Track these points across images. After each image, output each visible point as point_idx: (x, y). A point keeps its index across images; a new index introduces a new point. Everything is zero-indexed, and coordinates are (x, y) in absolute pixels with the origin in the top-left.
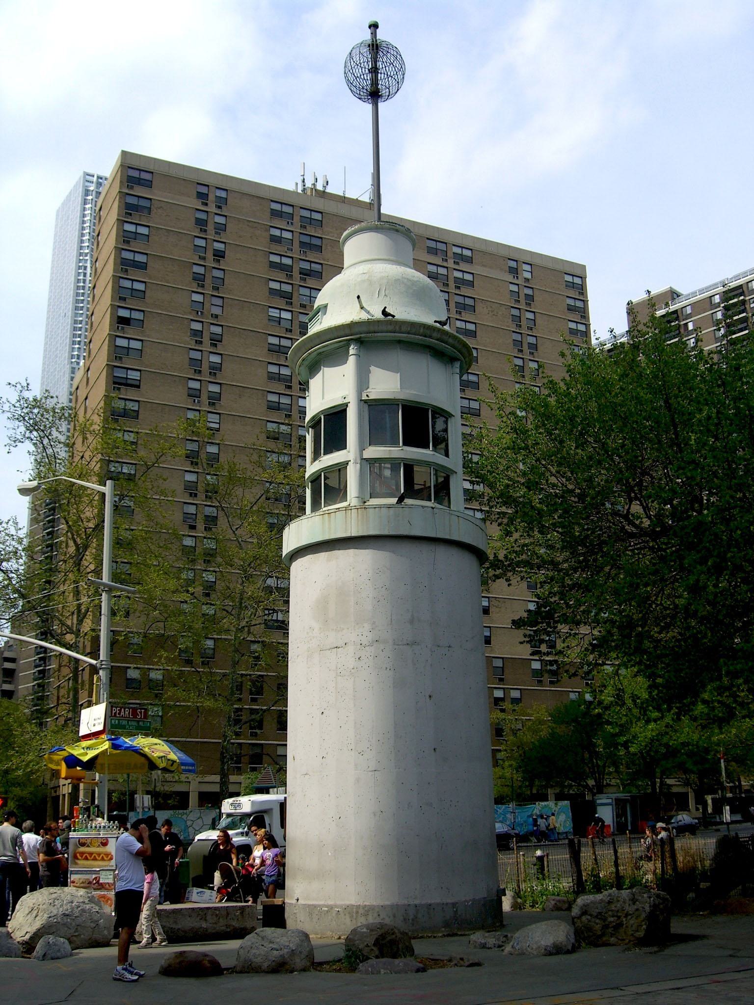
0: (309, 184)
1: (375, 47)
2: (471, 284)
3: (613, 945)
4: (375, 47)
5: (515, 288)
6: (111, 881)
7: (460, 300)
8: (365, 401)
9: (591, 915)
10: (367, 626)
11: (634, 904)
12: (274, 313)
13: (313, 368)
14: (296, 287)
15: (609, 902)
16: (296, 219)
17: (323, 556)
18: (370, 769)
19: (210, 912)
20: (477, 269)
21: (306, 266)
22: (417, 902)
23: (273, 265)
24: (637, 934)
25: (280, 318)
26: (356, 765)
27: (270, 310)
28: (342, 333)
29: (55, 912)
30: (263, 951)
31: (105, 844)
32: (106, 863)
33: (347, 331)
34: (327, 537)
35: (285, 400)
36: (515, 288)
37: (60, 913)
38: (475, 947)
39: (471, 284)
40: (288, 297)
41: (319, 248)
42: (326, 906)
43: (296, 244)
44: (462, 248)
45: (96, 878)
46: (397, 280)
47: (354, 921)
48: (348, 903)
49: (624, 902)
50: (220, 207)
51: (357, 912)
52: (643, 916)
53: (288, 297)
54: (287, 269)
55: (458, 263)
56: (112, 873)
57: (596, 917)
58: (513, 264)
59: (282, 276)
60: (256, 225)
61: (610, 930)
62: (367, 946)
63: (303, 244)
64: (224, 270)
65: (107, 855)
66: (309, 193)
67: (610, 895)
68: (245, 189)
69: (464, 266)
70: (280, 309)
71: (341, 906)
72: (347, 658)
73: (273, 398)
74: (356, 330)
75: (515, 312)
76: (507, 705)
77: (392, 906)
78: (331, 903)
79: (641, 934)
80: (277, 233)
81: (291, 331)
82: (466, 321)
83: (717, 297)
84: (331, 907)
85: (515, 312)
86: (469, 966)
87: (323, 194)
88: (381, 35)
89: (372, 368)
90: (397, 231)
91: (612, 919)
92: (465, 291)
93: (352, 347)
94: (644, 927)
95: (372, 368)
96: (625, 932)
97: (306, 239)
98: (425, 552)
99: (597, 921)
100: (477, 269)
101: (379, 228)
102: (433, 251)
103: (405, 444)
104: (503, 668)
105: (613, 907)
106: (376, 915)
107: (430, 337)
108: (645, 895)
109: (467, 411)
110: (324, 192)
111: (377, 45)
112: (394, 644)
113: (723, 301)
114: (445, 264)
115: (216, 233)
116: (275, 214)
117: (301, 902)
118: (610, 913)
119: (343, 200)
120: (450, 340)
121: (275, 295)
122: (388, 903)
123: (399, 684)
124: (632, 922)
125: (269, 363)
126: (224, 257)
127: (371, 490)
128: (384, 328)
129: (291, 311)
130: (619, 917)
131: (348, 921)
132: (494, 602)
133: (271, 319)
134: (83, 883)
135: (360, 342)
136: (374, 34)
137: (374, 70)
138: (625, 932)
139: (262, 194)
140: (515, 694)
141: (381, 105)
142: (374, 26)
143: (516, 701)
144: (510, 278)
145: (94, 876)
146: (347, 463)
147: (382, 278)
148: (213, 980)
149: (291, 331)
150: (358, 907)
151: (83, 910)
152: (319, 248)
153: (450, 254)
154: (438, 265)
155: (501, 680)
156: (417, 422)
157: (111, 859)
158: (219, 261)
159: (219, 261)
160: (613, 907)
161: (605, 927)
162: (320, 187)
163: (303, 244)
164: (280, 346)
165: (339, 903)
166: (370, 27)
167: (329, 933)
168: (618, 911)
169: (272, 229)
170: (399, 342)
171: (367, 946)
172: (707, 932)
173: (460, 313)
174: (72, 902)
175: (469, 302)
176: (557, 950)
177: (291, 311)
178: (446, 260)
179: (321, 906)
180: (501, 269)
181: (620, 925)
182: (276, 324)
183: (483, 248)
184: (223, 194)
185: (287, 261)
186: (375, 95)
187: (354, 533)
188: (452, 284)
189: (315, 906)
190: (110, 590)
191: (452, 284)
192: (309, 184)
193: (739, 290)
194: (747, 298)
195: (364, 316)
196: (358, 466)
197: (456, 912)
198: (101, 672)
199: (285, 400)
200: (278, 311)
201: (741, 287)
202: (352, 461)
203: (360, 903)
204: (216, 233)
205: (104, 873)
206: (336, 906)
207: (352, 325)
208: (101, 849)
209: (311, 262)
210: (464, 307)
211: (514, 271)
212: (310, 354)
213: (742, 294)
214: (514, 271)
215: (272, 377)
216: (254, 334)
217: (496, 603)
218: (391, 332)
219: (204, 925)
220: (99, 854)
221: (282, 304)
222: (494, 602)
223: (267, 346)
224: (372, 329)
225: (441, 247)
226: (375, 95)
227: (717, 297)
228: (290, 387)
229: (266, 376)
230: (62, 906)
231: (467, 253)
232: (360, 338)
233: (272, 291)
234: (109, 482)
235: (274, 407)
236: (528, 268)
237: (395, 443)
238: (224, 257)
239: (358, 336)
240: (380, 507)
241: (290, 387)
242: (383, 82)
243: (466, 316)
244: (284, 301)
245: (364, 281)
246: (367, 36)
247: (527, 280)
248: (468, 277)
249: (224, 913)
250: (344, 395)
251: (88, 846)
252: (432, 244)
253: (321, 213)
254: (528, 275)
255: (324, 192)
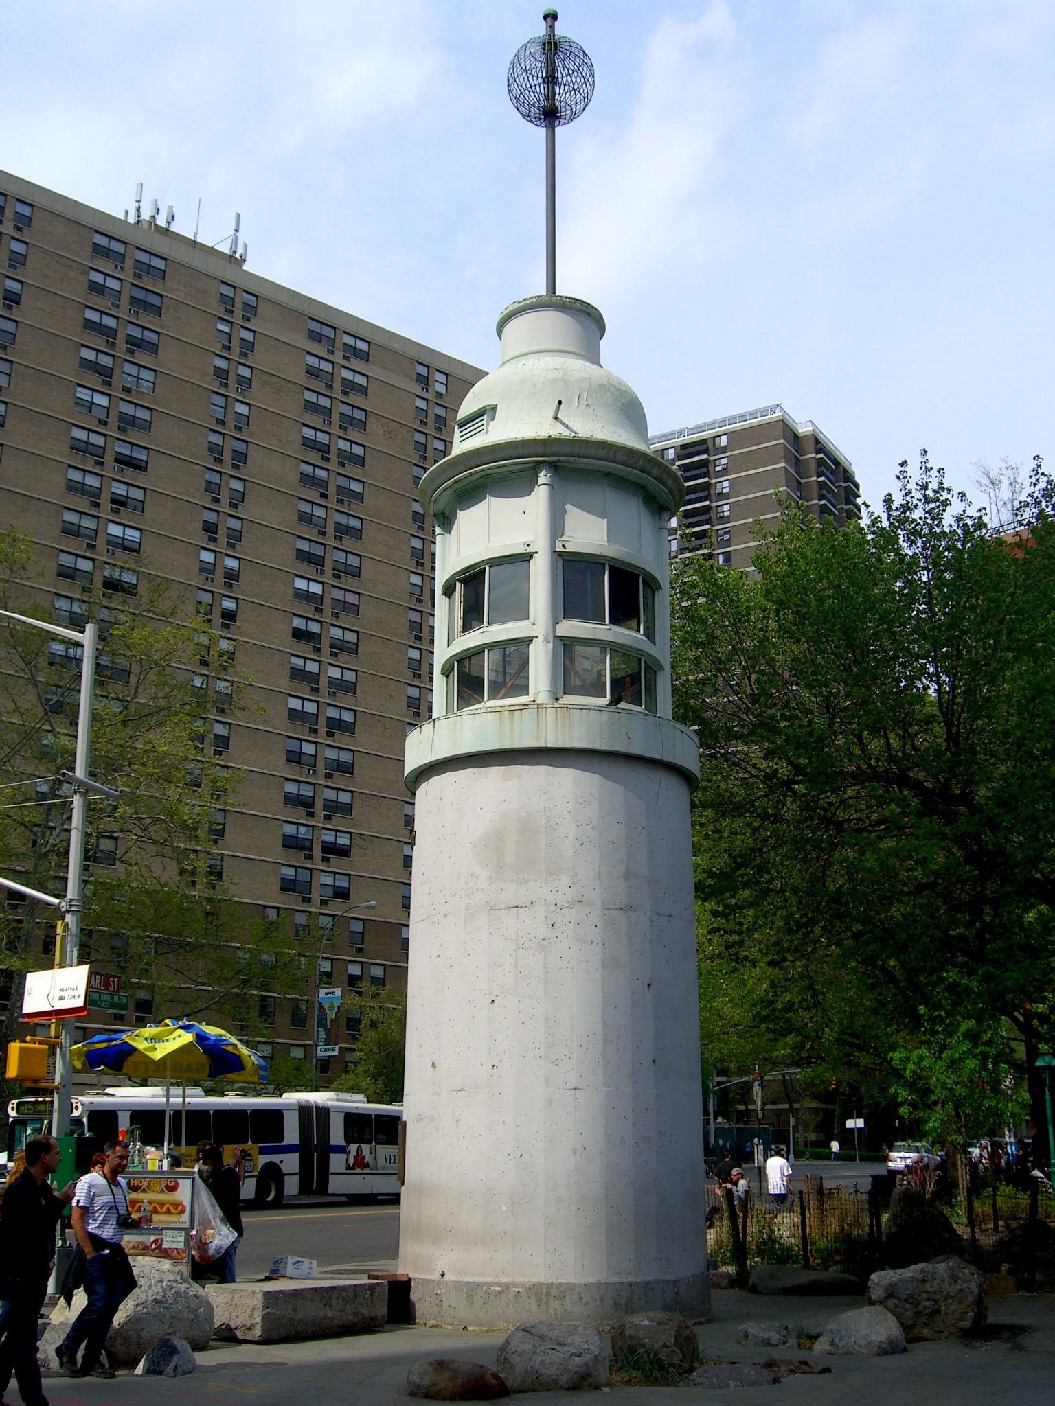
0: (146, 215)
1: (552, 47)
2: (364, 391)
3: (927, 1340)
4: (552, 47)
5: (421, 404)
6: (181, 1246)
7: (347, 410)
8: (560, 554)
9: (899, 1299)
10: (565, 879)
11: (955, 1282)
12: (84, 394)
13: (469, 494)
14: (118, 361)
15: (923, 1281)
16: (129, 263)
17: (494, 773)
18: (568, 1086)
19: (335, 1294)
20: (372, 370)
21: (136, 333)
22: (631, 1279)
23: (89, 324)
24: (961, 1324)
25: (92, 402)
26: (547, 1080)
27: (79, 389)
28: (532, 451)
29: (144, 1298)
30: (555, 1357)
31: (172, 1189)
32: (175, 1218)
33: (540, 450)
34: (507, 744)
35: (88, 523)
36: (421, 404)
37: (151, 1299)
38: (756, 1344)
39: (364, 391)
40: (106, 374)
41: (158, 311)
42: (499, 1285)
43: (125, 299)
44: (356, 337)
45: (155, 1241)
46: (602, 386)
47: (543, 1307)
48: (534, 1280)
49: (942, 1281)
50: (20, 229)
51: (548, 1294)
52: (970, 1299)
53: (106, 374)
54: (109, 333)
55: (348, 359)
56: (183, 1233)
57: (906, 1300)
58: (423, 371)
59: (100, 343)
60: (69, 263)
61: (923, 1319)
62: (665, 1345)
63: (134, 300)
64: (16, 322)
65: (176, 1205)
66: (145, 226)
67: (923, 1271)
68: (59, 208)
69: (355, 364)
70: (93, 390)
71: (522, 1285)
72: (534, 924)
73: (71, 518)
74: (555, 449)
75: (420, 438)
76: (365, 986)
77: (598, 1286)
78: (504, 1280)
79: (967, 1324)
80: (99, 278)
81: (106, 423)
82: (352, 442)
83: (672, 451)
84: (506, 1287)
85: (420, 438)
86: (820, 1373)
87: (166, 232)
88: (561, 29)
89: (569, 507)
90: (589, 315)
91: (927, 1303)
92: (354, 399)
93: (544, 472)
94: (971, 1314)
95: (569, 507)
96: (944, 1323)
97: (140, 295)
98: (642, 776)
99: (907, 1306)
100: (372, 370)
101: (571, 308)
102: (315, 337)
103: (614, 620)
104: (363, 934)
105: (928, 1287)
106: (576, 1297)
107: (649, 474)
108: (966, 1271)
109: (342, 567)
110: (167, 230)
111: (555, 43)
112: (604, 908)
113: (679, 458)
114: (330, 357)
115: (11, 266)
116: (98, 250)
117: (446, 1277)
118: (925, 1295)
119: (194, 244)
120: (670, 482)
121: (89, 368)
122: (592, 1280)
123: (610, 964)
124: (953, 1307)
125: (70, 466)
126: (18, 303)
127: (569, 679)
128: (592, 452)
129: (109, 395)
130: (936, 1301)
131: (534, 1307)
132: (358, 841)
133: (79, 402)
134: (134, 1247)
135: (555, 467)
136: (552, 27)
137: (551, 80)
138: (944, 1323)
139: (84, 219)
140: (377, 972)
141: (559, 131)
142: (551, 17)
143: (376, 981)
144: (417, 389)
145: (153, 1238)
146: (529, 640)
147: (582, 380)
148: (506, 1400)
149: (106, 423)
150: (550, 1286)
151: (178, 1294)
152: (158, 311)
153: (338, 344)
154: (321, 358)
155: (360, 950)
156: (626, 591)
157: (183, 1211)
158: (10, 308)
159: (10, 308)
160: (928, 1287)
161: (918, 1313)
162: (161, 221)
163: (134, 300)
164: (87, 443)
165: (518, 1279)
166: (545, 18)
167: (502, 1325)
168: (935, 1293)
169: (92, 272)
170: (607, 474)
171: (665, 1345)
172: (1026, 1321)
173: (345, 429)
174: (162, 1281)
175: (359, 415)
176: (890, 1349)
177: (109, 395)
178: (333, 353)
179: (489, 1285)
180: (407, 376)
181: (938, 1311)
182: (86, 411)
183: (385, 342)
184: (26, 211)
185: (110, 322)
186: (550, 116)
187: (550, 743)
188: (337, 386)
189: (478, 1285)
190: (86, 791)
191: (337, 386)
192: (146, 215)
193: (702, 446)
194: (712, 458)
195: (558, 431)
196: (550, 645)
197: (677, 1293)
198: (68, 918)
199: (88, 523)
200: (89, 392)
201: (705, 441)
202: (541, 638)
203: (553, 1280)
204: (11, 266)
205: (170, 1233)
206: (515, 1285)
207: (550, 441)
208: (167, 1197)
209: (144, 328)
210: (352, 421)
211: (424, 381)
212: (471, 474)
213: (706, 451)
214: (424, 381)
215: (72, 487)
216: (52, 420)
217: (361, 842)
218: (600, 459)
219: (330, 1314)
220: (162, 1204)
221: (96, 381)
222: (358, 841)
223: (69, 441)
224: (576, 451)
225: (328, 332)
226: (550, 116)
227: (672, 451)
228: (97, 505)
229: (63, 484)
230: (150, 1286)
231: (362, 346)
232: (558, 461)
233: (85, 363)
234: (90, 628)
235: (72, 531)
236: (442, 378)
237: (599, 618)
238: (18, 303)
239: (555, 458)
240: (589, 708)
241: (97, 505)
242: (564, 96)
243: (353, 434)
244: (100, 379)
245: (556, 380)
246: (541, 29)
247: (440, 395)
248: (361, 380)
249: (351, 1294)
250: (529, 539)
251: (144, 1191)
252: (316, 327)
253: (165, 259)
254: (441, 389)
255: (167, 230)
